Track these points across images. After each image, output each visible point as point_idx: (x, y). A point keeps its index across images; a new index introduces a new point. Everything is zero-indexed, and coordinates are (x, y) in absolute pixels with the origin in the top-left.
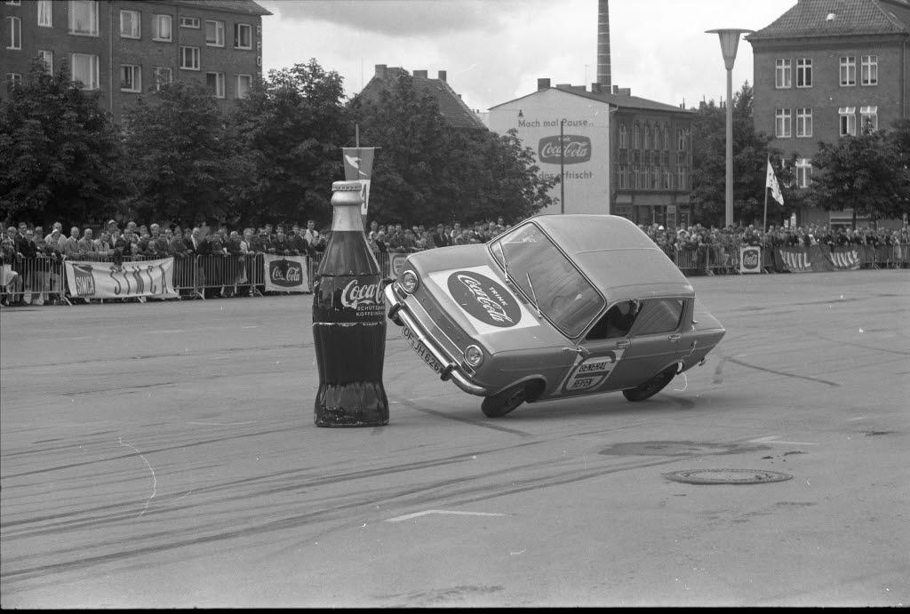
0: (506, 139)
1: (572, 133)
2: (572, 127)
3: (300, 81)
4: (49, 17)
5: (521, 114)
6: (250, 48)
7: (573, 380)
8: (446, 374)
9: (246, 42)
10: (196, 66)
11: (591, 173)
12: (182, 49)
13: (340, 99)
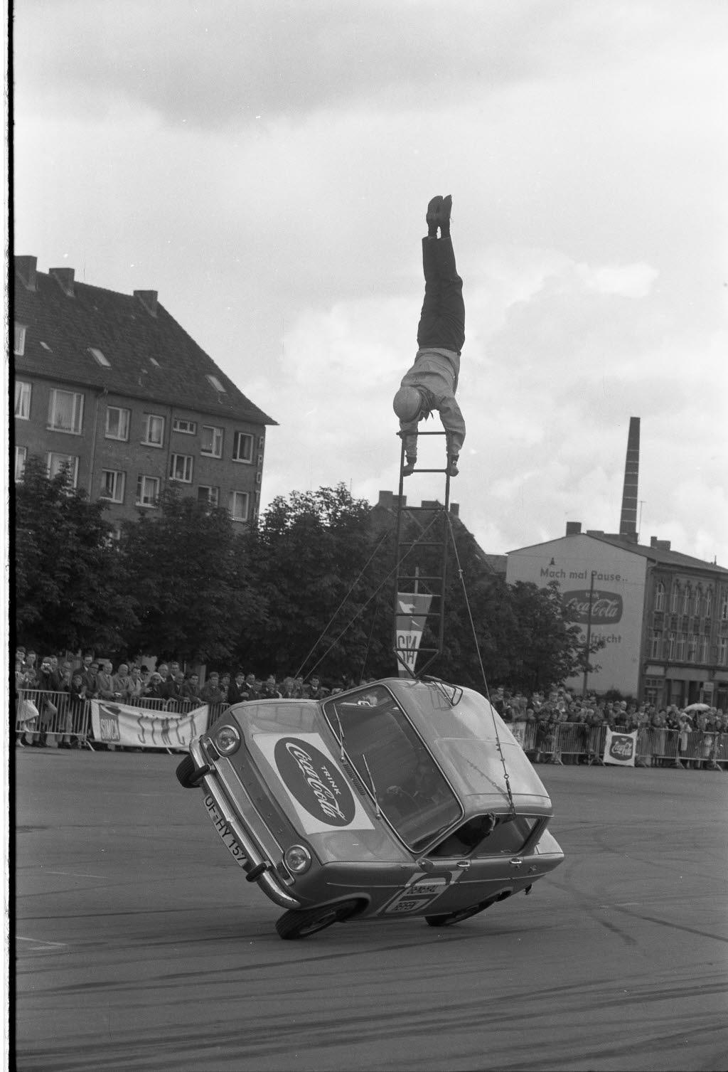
0: (545, 592)
1: (602, 589)
2: (603, 582)
3: (324, 507)
4: (27, 410)
5: (552, 563)
6: (249, 462)
7: (396, 903)
8: (254, 874)
9: (245, 455)
10: (187, 478)
11: (620, 638)
12: (173, 457)
13: (369, 533)
